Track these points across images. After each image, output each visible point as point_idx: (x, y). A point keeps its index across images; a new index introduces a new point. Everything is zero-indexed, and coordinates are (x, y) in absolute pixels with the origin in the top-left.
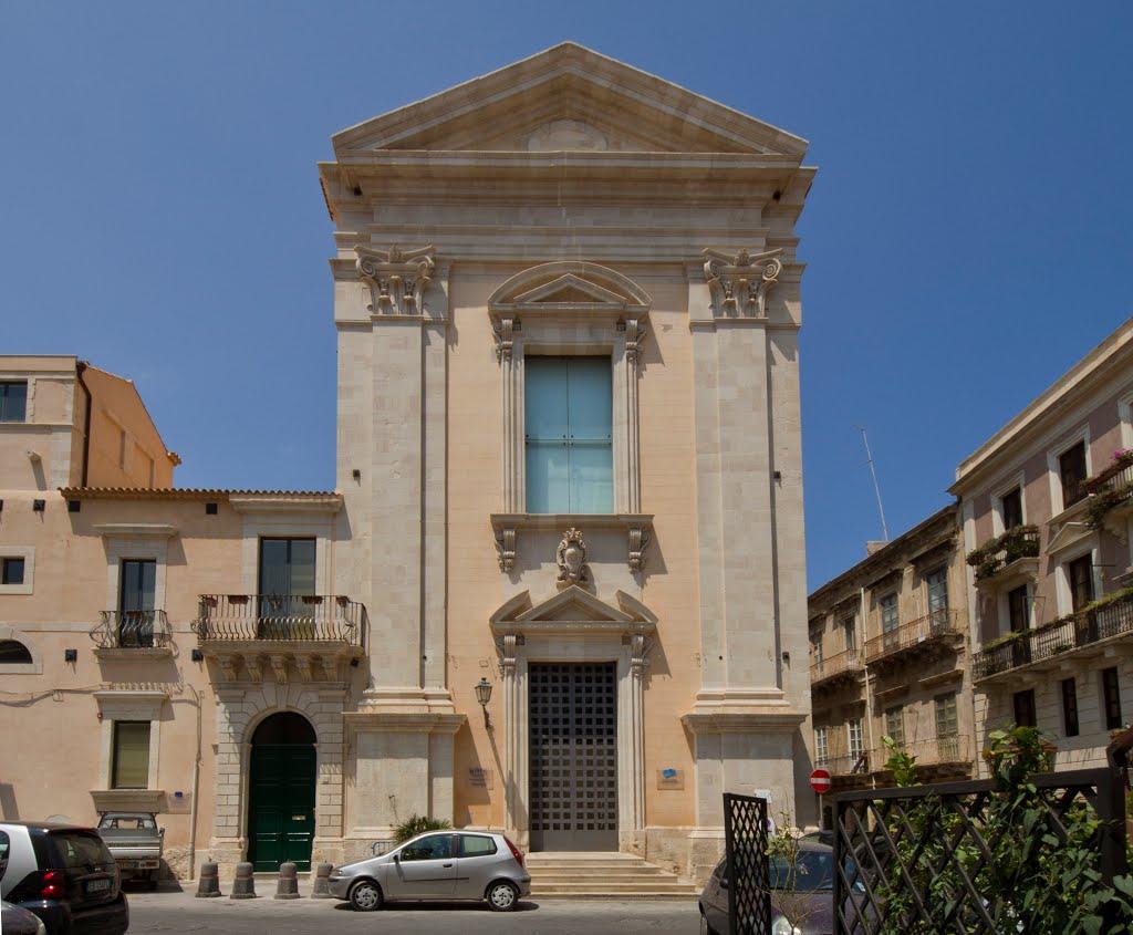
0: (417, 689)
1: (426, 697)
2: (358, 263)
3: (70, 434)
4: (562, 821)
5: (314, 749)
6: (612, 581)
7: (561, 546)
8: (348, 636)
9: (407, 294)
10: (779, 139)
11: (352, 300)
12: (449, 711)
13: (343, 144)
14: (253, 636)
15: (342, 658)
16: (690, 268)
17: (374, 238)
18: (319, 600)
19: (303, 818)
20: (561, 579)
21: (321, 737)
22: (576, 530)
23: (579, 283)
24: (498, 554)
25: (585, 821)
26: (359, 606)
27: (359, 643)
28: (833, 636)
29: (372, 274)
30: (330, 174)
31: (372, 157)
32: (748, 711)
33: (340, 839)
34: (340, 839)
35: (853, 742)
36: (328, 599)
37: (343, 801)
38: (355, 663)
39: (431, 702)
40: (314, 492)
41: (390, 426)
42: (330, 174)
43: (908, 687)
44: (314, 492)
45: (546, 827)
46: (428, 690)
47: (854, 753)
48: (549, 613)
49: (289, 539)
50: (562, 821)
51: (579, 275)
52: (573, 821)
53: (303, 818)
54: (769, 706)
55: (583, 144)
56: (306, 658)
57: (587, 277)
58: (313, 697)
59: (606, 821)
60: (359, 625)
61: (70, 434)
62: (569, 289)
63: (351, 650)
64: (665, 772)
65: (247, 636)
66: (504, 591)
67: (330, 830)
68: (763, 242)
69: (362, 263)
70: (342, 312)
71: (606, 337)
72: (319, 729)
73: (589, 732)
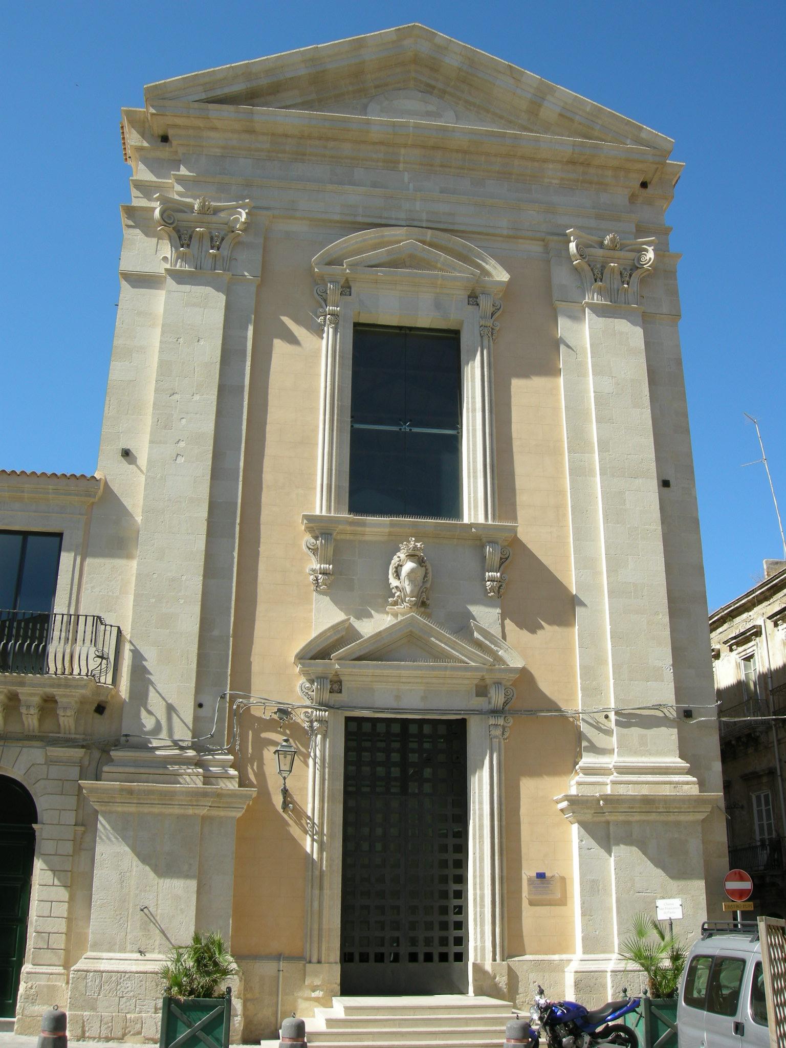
2: (157, 213)
3: (517, 384)
5: (33, 832)
7: (395, 561)
8: (96, 672)
10: (643, 135)
11: (150, 253)
15: (83, 701)
22: (416, 541)
24: (13, 1034)
26: (115, 630)
27: (109, 681)
29: (178, 228)
32: (645, 791)
35: (760, 812)
38: (100, 709)
41: (176, 397)
48: (379, 652)
49: (25, 534)
51: (424, 242)
54: (670, 783)
55: (429, 114)
56: (36, 700)
57: (430, 245)
59: (454, 949)
61: (517, 384)
63: (99, 689)
66: (324, 616)
67: (48, 956)
69: (162, 213)
70: (130, 261)
72: (42, 804)
73: (444, 941)
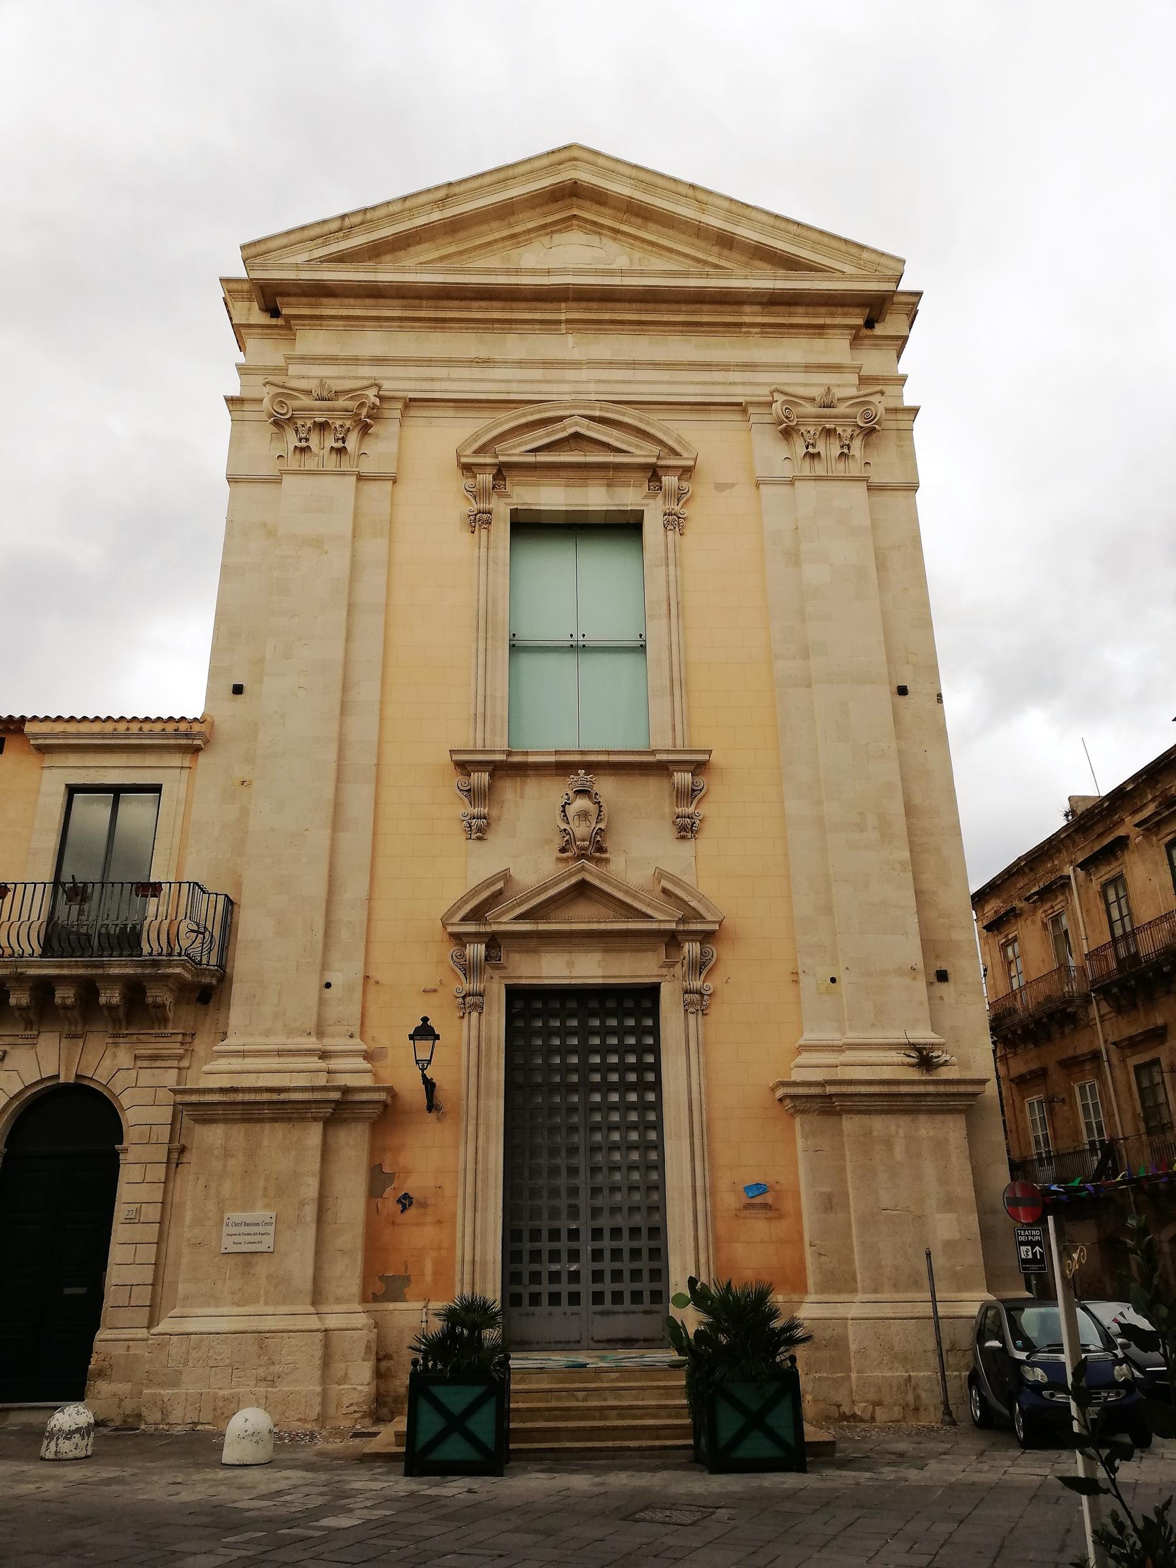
0: (311, 1042)
1: (324, 1055)
4: (564, 1288)
5: (116, 1155)
6: (644, 853)
9: (337, 440)
12: (367, 1081)
13: (252, 252)
14: (38, 950)
16: (751, 410)
17: (293, 370)
18: (154, 889)
19: (68, 1291)
20: (563, 850)
21: (131, 1135)
23: (630, 444)
25: (608, 1287)
26: (221, 899)
28: (1031, 937)
30: (232, 289)
31: (289, 268)
33: (142, 1333)
34: (142, 1333)
35: (1089, 1126)
36: (20, 888)
37: (158, 1257)
39: (334, 1064)
40: (103, 717)
42: (232, 289)
43: (1165, 1028)
44: (103, 717)
45: (535, 1299)
46: (331, 1044)
47: (1092, 1143)
50: (564, 1288)
52: (586, 1287)
53: (68, 1291)
58: (124, 1057)
60: (217, 934)
62: (577, 436)
64: (747, 1189)
65: (28, 951)
68: (854, 379)
71: (628, 497)
